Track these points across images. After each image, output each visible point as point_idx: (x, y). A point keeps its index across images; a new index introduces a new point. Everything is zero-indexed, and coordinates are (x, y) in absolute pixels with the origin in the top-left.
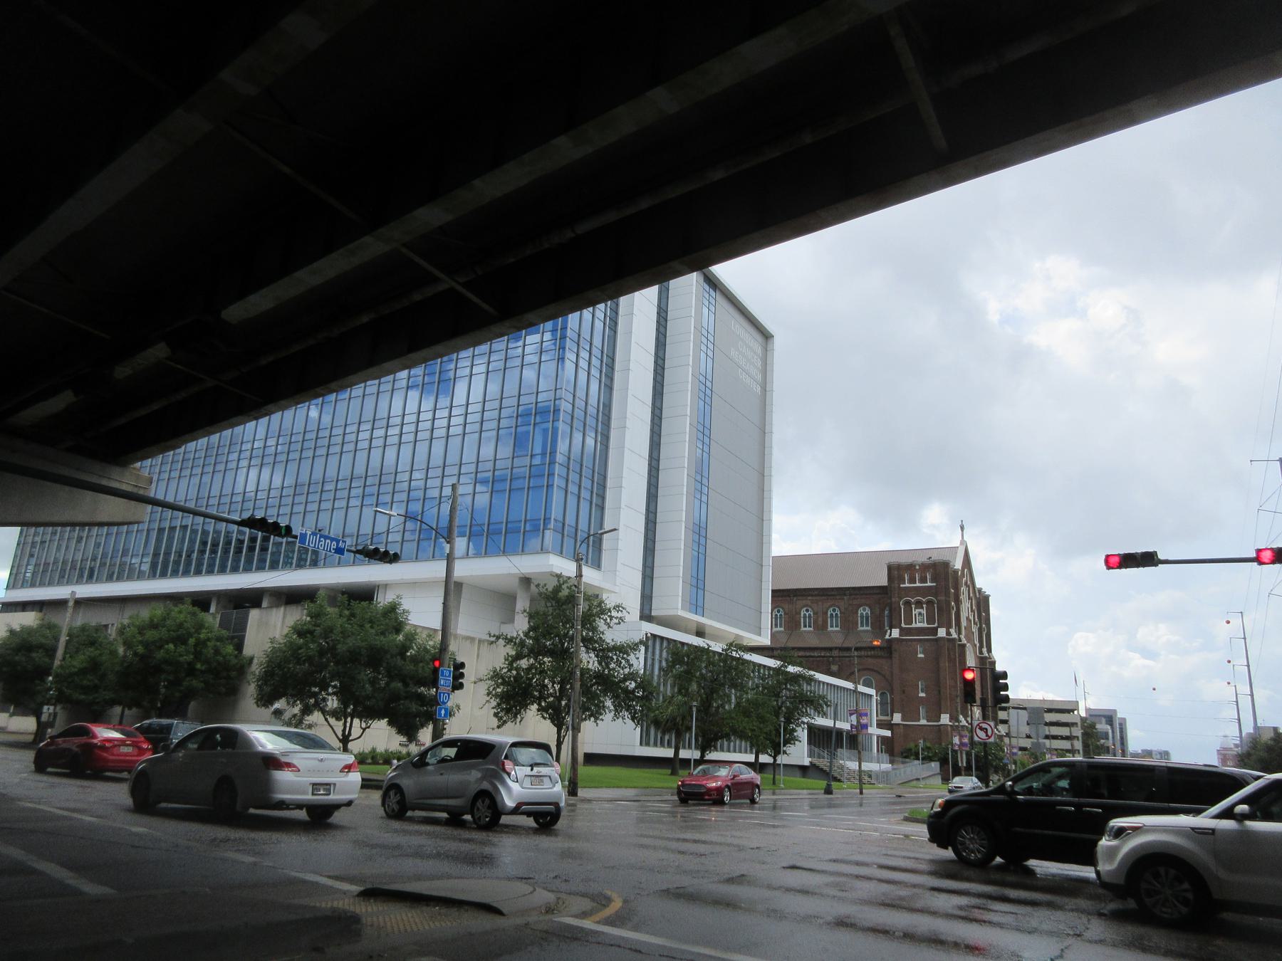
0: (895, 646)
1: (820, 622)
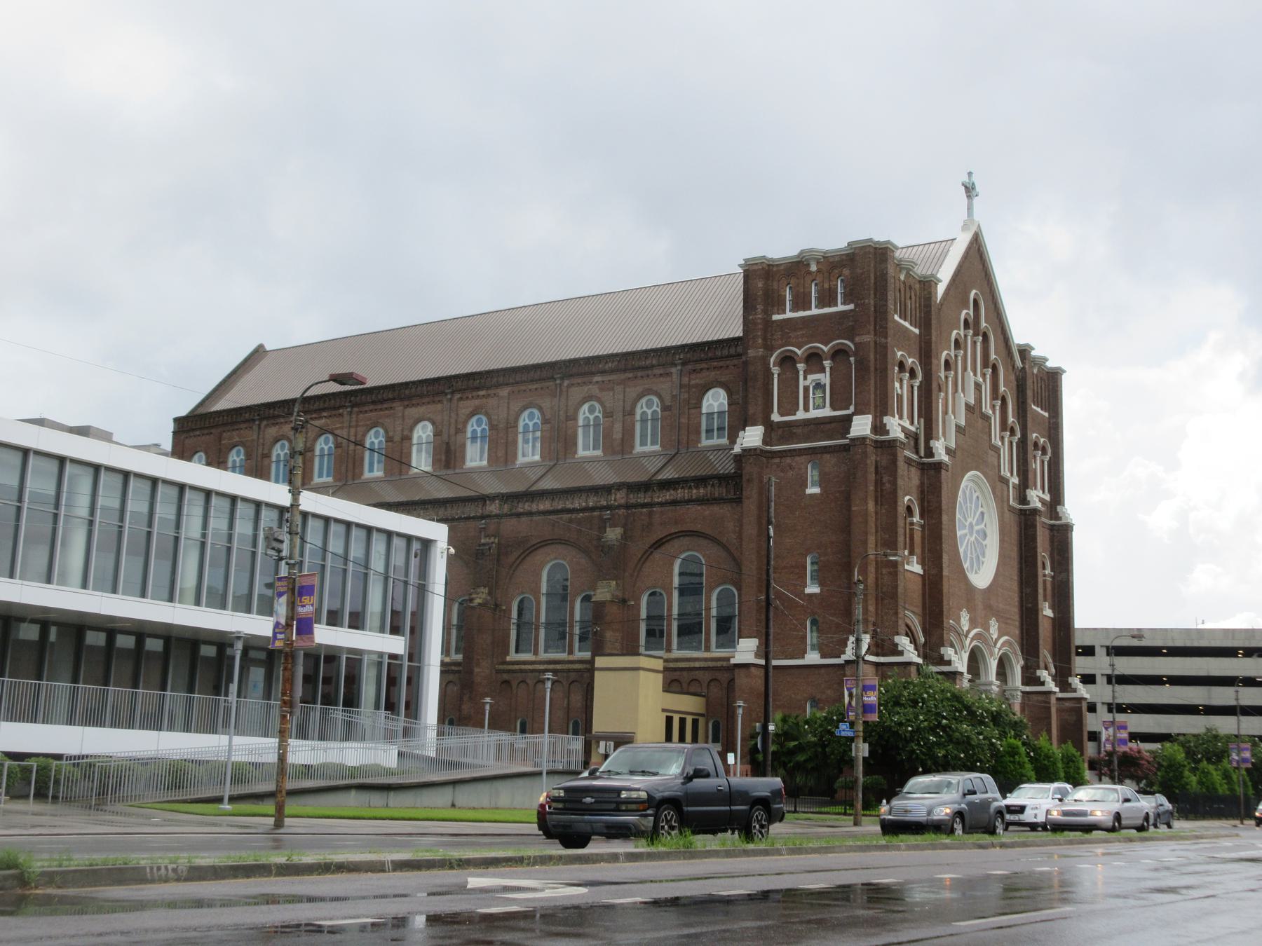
0: (750, 469)
1: (617, 435)
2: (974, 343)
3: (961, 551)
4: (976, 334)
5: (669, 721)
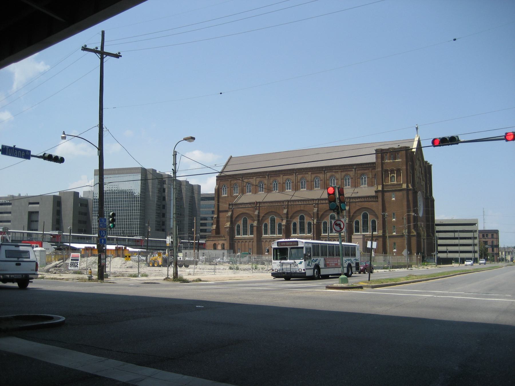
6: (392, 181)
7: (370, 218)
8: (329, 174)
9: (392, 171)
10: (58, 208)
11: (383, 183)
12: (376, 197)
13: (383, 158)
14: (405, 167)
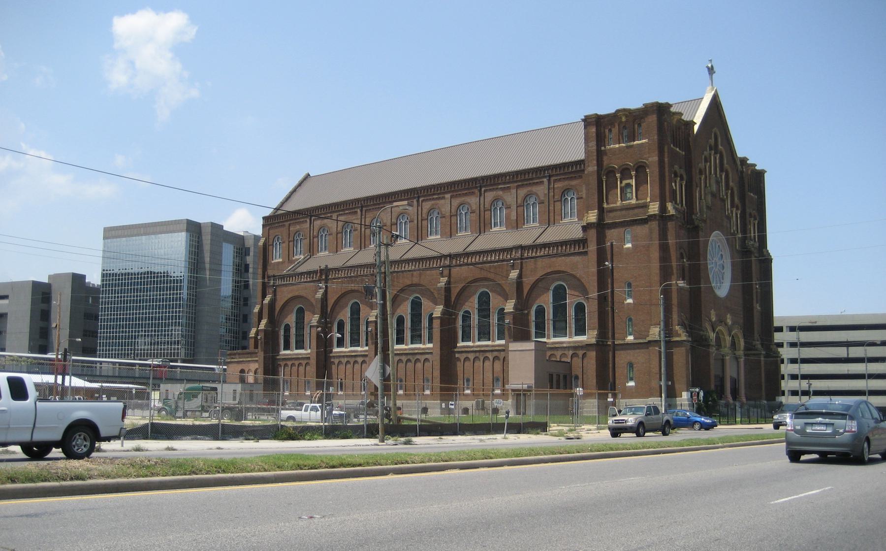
2: (715, 158)
3: (711, 276)
4: (716, 153)
5: (551, 376)
6: (627, 197)
7: (571, 301)
8: (490, 196)
9: (625, 172)
10: (44, 306)
11: (600, 202)
12: (583, 242)
13: (601, 140)
14: (656, 158)
